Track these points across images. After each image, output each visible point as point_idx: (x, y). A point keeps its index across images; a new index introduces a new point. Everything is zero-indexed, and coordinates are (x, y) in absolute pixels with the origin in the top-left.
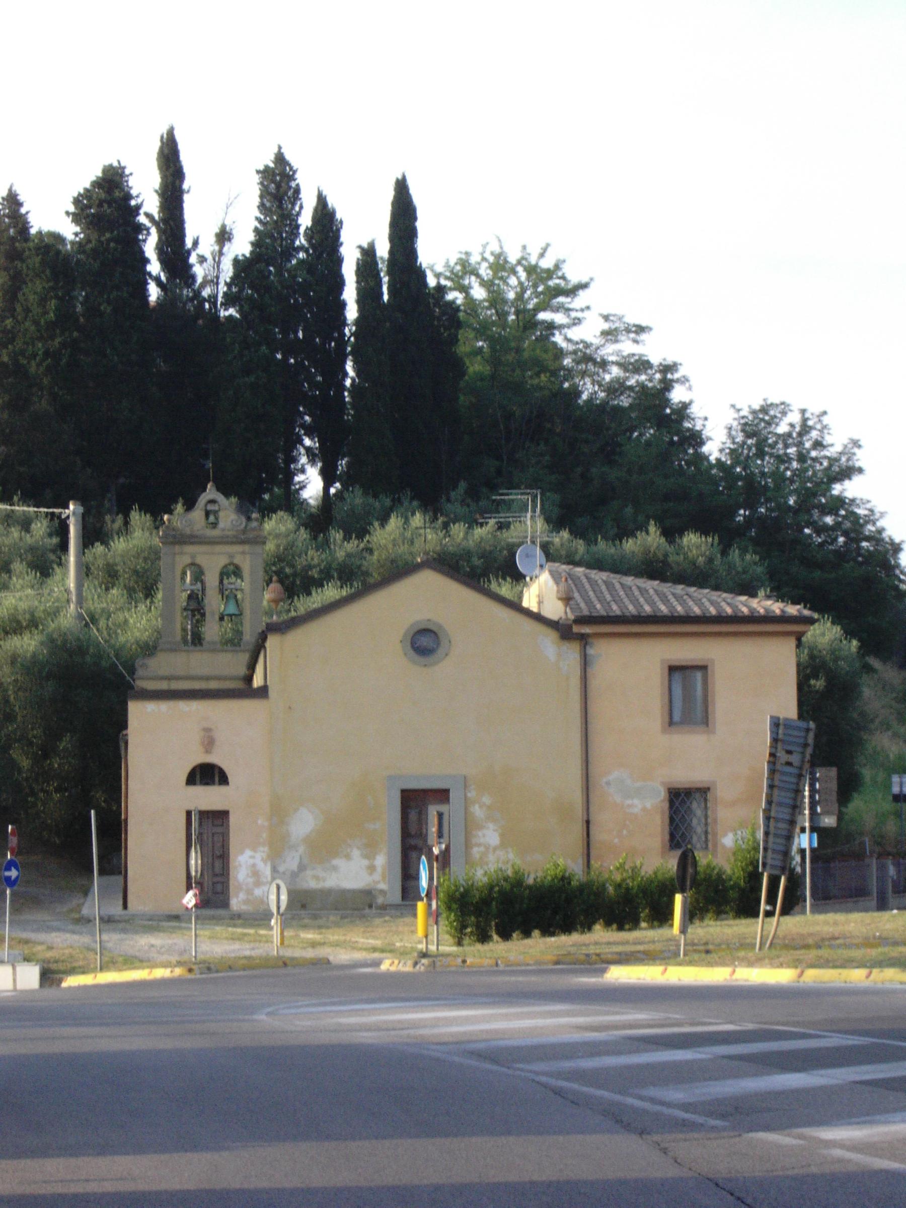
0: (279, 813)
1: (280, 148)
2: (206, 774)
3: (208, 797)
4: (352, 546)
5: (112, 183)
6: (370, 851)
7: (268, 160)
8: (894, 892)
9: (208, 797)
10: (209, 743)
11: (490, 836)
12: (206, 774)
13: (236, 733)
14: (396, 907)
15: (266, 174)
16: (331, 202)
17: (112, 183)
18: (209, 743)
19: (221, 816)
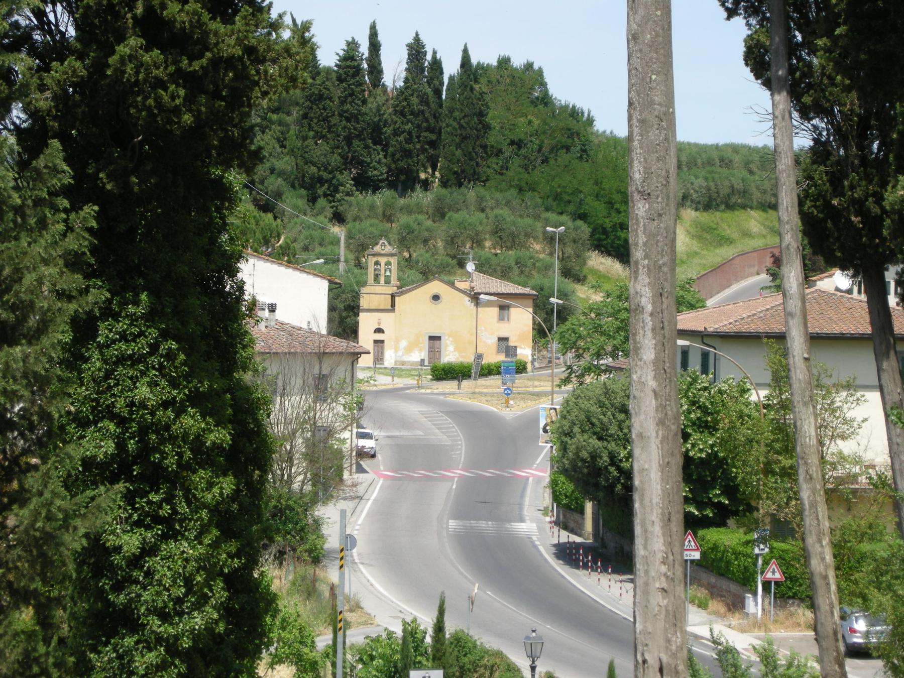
0: (397, 341)
1: (417, 35)
2: (379, 331)
3: (379, 337)
4: (349, 185)
5: (352, 45)
6: (420, 350)
7: (410, 40)
8: (339, 241)
9: (379, 337)
10: (379, 324)
11: (451, 348)
12: (379, 331)
13: (386, 321)
14: (807, 331)
15: (410, 46)
16: (421, 37)
17: (352, 45)
18: (379, 324)
19: (382, 342)
